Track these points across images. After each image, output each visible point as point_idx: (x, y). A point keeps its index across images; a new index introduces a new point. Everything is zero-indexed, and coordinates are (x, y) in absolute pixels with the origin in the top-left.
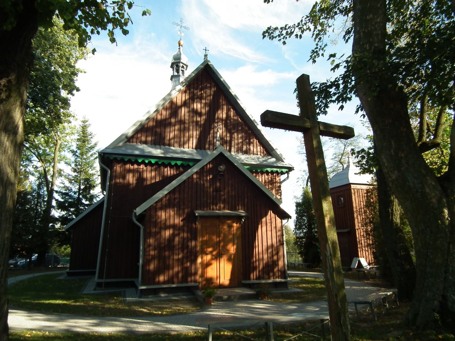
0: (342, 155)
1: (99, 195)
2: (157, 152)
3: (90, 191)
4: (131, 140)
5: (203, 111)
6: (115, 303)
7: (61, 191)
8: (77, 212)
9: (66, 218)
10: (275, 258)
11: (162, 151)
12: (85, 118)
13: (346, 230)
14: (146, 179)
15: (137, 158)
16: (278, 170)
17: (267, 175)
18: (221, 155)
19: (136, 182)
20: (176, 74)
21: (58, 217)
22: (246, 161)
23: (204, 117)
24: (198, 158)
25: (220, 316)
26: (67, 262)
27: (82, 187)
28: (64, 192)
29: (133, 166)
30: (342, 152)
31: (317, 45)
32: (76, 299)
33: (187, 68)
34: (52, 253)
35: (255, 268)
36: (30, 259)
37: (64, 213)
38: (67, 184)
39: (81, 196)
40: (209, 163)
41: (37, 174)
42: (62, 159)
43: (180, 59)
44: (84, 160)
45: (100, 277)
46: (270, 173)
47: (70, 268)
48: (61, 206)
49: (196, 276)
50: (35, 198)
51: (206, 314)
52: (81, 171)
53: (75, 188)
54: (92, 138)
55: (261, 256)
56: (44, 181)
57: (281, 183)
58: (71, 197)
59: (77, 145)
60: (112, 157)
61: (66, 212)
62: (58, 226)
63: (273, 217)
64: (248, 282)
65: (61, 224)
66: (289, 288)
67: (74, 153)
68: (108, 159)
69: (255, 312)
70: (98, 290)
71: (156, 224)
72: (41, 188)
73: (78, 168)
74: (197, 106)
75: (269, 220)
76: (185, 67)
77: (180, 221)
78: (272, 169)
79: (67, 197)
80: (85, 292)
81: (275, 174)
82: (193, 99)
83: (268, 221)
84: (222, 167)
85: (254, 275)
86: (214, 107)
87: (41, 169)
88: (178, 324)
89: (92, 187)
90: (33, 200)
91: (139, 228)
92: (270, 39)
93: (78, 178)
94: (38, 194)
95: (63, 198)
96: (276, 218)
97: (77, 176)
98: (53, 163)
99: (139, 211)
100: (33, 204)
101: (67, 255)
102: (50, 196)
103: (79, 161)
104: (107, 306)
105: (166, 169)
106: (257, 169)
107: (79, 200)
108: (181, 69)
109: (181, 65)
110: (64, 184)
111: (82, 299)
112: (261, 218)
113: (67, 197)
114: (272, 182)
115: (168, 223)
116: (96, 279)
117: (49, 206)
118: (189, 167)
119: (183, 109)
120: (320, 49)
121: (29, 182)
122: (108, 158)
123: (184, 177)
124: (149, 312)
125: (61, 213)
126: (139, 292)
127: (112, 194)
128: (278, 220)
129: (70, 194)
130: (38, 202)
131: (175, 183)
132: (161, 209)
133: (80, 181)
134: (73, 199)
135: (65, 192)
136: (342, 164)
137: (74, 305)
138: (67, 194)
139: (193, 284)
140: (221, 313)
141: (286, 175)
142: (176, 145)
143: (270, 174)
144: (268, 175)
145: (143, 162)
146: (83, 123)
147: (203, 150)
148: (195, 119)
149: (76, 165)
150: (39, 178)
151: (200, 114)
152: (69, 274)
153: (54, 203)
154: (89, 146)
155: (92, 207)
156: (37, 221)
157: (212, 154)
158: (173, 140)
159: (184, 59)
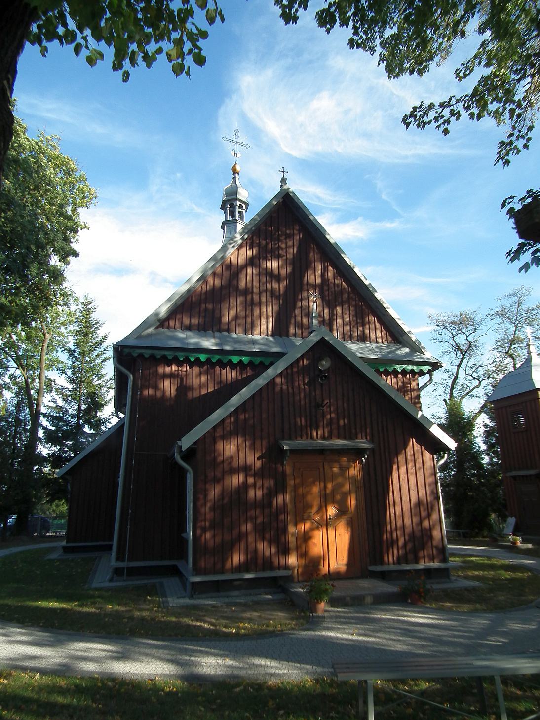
0: (512, 342)
1: (109, 419)
2: (209, 343)
3: (96, 413)
4: (166, 324)
5: (283, 272)
6: (151, 610)
7: (52, 414)
8: (75, 448)
9: (60, 456)
10: (426, 524)
11: (217, 341)
12: (87, 298)
13: (532, 472)
14: (192, 388)
15: (176, 354)
16: (415, 368)
17: (395, 377)
18: (322, 341)
19: (175, 393)
20: (229, 218)
21: (47, 456)
22: (361, 353)
23: (285, 283)
24: (275, 350)
25: (351, 643)
26: (60, 527)
27: (83, 407)
28: (55, 415)
29: (170, 368)
30: (511, 337)
31: (514, 128)
32: (81, 598)
33: (247, 208)
34: (38, 513)
35: (393, 543)
36: (6, 523)
37: (56, 448)
38: (60, 402)
39: (81, 422)
40: (302, 357)
41: (15, 388)
42: (53, 363)
43: (236, 193)
44: (85, 365)
45: (118, 559)
46: (400, 373)
47: (68, 537)
48: (51, 437)
49: (287, 558)
50: (12, 426)
51: (322, 636)
52: (82, 382)
53: (72, 409)
54: (98, 328)
55: (399, 523)
56: (26, 399)
57: (420, 389)
58: (66, 423)
59: (76, 340)
60: (136, 353)
61: (58, 447)
62: (47, 469)
63: (418, 450)
64: (379, 568)
65: (52, 467)
66: (453, 578)
67: (71, 353)
68: (127, 355)
69: (415, 634)
70: (116, 581)
71: (214, 463)
72: (20, 410)
73: (77, 377)
74: (273, 265)
75: (411, 455)
76: (244, 206)
77: (256, 459)
78: (404, 366)
79: (60, 424)
80: (95, 585)
81: (408, 375)
82: (265, 253)
83: (409, 458)
84: (325, 364)
85: (391, 557)
86: (300, 265)
87: (21, 380)
88: (277, 660)
89: (99, 406)
90: (9, 429)
91: (183, 473)
92: (418, 128)
93: (77, 394)
94: (17, 419)
95: (53, 425)
96: (424, 453)
97: (75, 389)
98: (39, 370)
99: (186, 442)
100: (9, 436)
101: (61, 516)
102: (35, 423)
103: (79, 365)
104: (137, 614)
105: (224, 371)
106: (383, 365)
107: (79, 427)
108: (237, 210)
109: (238, 203)
110: (55, 402)
111: (92, 600)
112: (397, 454)
113: (60, 424)
114: (404, 389)
115: (235, 464)
116: (114, 563)
117: (34, 440)
118: (263, 367)
119: (249, 271)
120: (518, 135)
121: (3, 400)
122: (130, 354)
123: (260, 382)
124: (214, 628)
125: (51, 449)
126: (189, 587)
127: (136, 415)
128: (428, 455)
129: (65, 418)
130: (16, 433)
131: (245, 393)
132: (223, 438)
133: (80, 397)
134: (70, 426)
135: (58, 415)
136: (513, 359)
137: (80, 612)
138: (59, 419)
139: (282, 573)
140: (349, 633)
141: (428, 376)
142: (239, 330)
143: (400, 375)
144: (396, 377)
145: (187, 361)
146: (83, 306)
147: (285, 338)
148: (269, 286)
149: (74, 373)
150: (18, 394)
151: (278, 278)
152: (66, 549)
153: (41, 433)
154: (94, 341)
155: (99, 440)
156: (16, 462)
157: (300, 344)
158: (234, 322)
159: (243, 194)
